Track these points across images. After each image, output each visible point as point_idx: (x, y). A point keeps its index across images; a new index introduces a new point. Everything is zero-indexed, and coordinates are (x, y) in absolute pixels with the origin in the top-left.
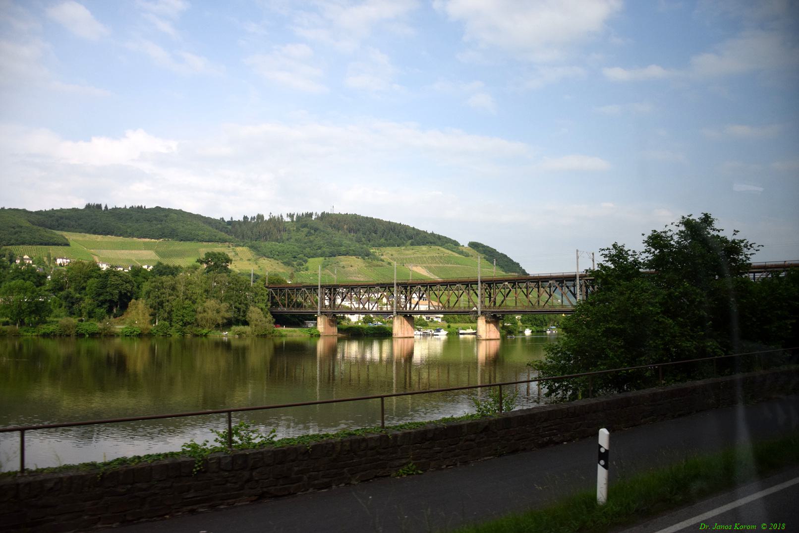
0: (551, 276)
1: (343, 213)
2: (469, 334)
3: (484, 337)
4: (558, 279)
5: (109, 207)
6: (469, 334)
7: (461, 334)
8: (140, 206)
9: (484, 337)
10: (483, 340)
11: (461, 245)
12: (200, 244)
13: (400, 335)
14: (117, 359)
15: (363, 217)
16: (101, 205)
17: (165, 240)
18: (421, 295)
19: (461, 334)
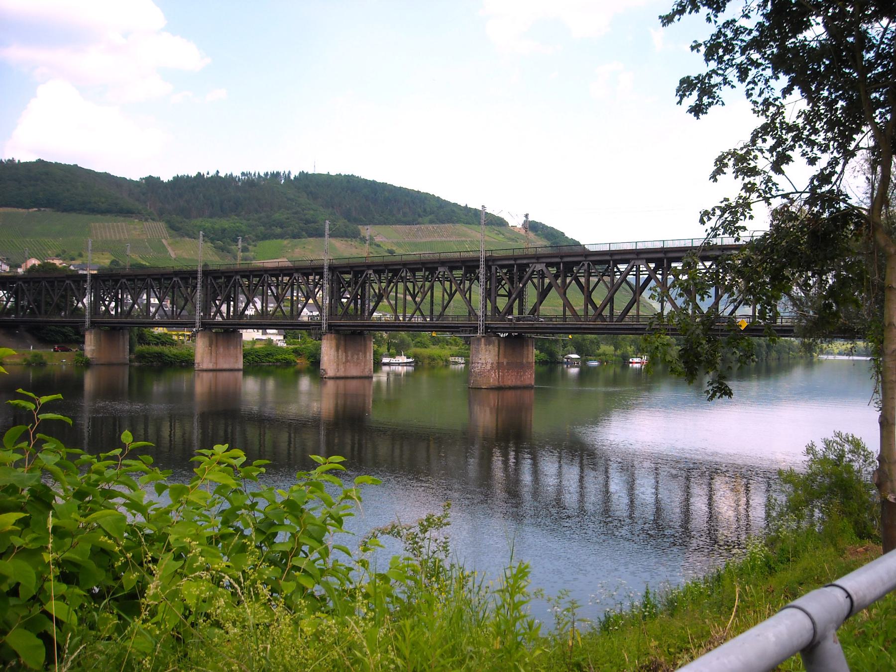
0: (263, 267)
1: (333, 173)
2: (399, 364)
3: (331, 372)
4: (273, 272)
5: (222, 175)
6: (399, 364)
7: (385, 364)
8: (11, 159)
9: (331, 372)
10: (330, 378)
11: (525, 219)
12: (91, 217)
13: (205, 366)
14: (392, 385)
15: (366, 181)
16: (199, 173)
17: (39, 210)
18: (393, 302)
19: (385, 364)
